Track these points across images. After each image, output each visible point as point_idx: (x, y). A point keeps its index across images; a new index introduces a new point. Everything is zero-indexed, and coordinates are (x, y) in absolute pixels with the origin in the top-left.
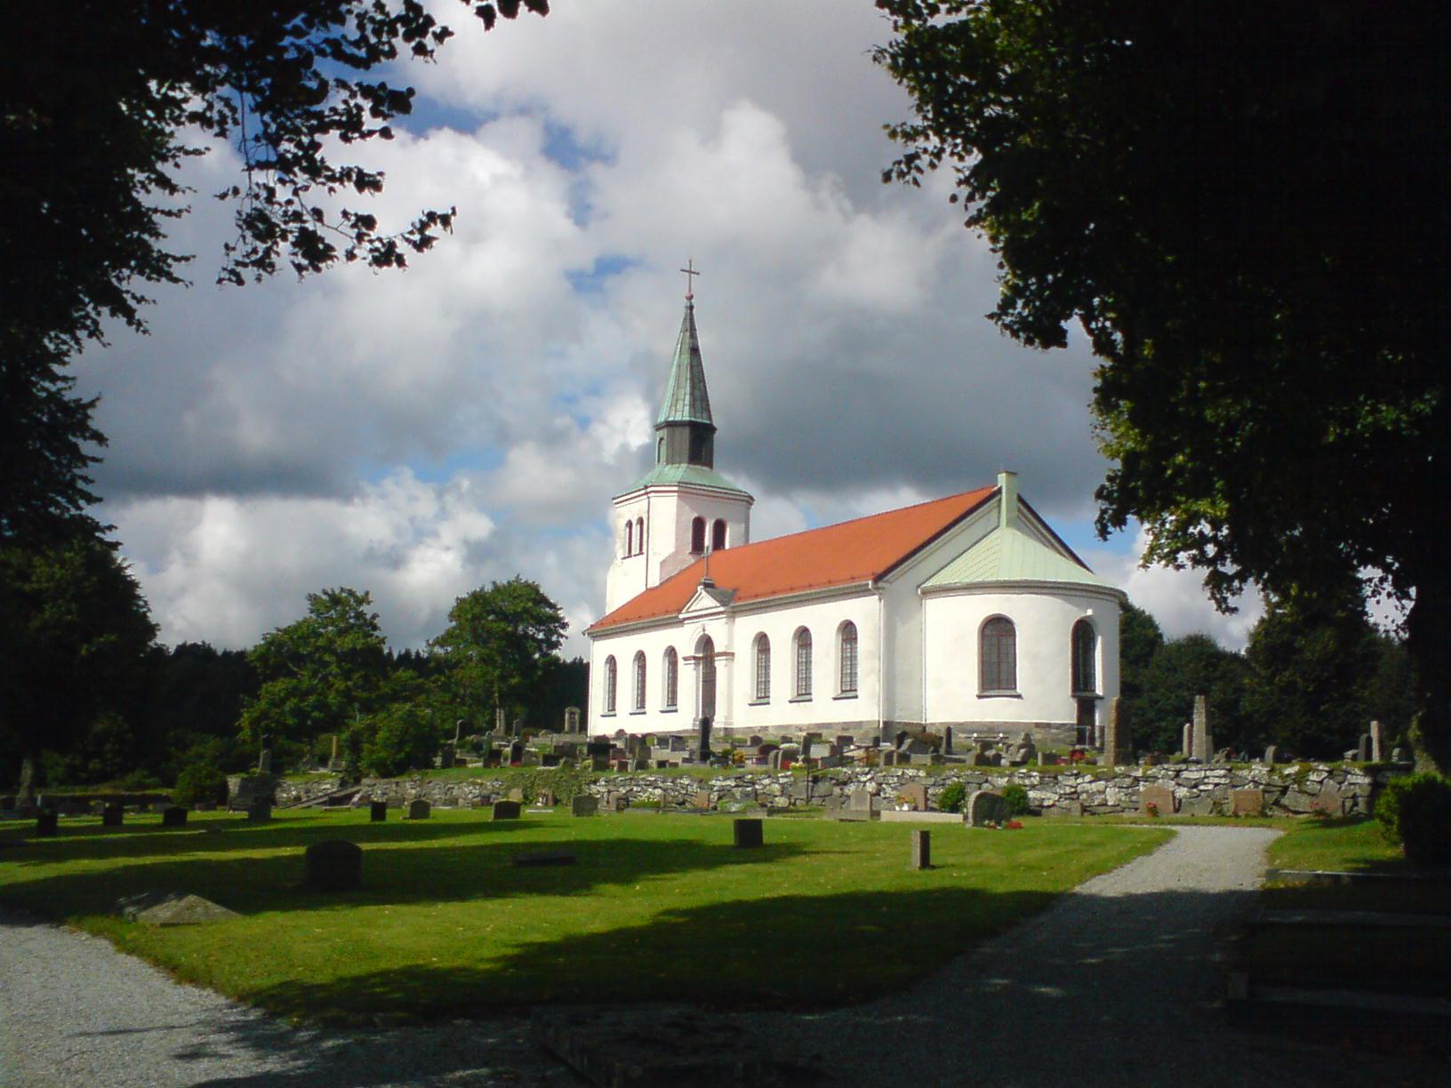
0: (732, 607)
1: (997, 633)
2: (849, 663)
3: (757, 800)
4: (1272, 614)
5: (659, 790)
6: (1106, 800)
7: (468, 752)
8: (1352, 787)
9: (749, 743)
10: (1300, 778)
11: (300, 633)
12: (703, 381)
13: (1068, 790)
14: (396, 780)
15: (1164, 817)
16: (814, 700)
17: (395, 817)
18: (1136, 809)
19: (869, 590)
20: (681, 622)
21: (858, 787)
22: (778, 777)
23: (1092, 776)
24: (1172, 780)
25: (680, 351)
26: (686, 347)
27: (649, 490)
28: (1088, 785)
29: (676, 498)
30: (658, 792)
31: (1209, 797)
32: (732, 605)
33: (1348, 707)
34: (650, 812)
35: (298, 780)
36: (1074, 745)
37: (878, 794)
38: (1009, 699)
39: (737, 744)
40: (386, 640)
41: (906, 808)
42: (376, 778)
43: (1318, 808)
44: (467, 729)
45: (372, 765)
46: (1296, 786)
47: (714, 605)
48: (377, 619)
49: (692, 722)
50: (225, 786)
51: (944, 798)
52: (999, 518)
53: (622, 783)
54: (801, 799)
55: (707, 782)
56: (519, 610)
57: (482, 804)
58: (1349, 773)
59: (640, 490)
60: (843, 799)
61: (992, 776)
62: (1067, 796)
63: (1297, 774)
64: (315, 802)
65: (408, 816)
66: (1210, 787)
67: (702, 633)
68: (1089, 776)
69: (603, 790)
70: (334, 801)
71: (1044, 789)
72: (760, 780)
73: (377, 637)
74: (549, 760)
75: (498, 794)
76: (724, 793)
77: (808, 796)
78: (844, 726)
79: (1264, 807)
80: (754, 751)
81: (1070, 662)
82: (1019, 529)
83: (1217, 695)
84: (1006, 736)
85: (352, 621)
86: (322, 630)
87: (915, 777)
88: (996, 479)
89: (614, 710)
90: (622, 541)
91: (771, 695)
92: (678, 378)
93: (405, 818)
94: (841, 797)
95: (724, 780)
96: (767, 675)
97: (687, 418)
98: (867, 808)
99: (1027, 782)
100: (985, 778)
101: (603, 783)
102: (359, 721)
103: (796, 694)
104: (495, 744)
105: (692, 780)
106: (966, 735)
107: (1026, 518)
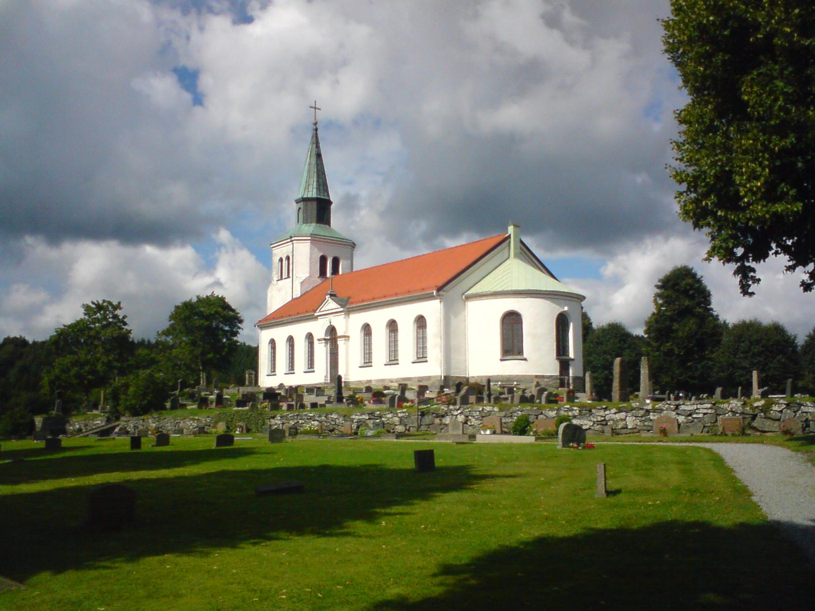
0: (348, 308)
1: (512, 321)
2: (393, 344)
3: (384, 428)
4: (659, 310)
5: (316, 422)
6: (626, 425)
7: (186, 399)
8: (805, 414)
9: (364, 391)
10: (766, 409)
11: (78, 327)
12: (324, 173)
13: (599, 419)
14: (142, 417)
15: (670, 436)
16: (428, 361)
17: (148, 445)
18: (648, 431)
19: (434, 296)
20: (316, 318)
21: (452, 418)
22: (398, 413)
23: (617, 409)
24: (674, 411)
25: (310, 156)
26: (314, 153)
27: (293, 239)
28: (614, 415)
29: (309, 244)
30: (316, 423)
31: (700, 422)
32: (348, 307)
33: (703, 363)
34: (315, 438)
35: (79, 418)
36: (558, 388)
37: (466, 423)
38: (520, 361)
39: (356, 391)
40: (132, 332)
41: (488, 432)
42: (129, 416)
43: (785, 429)
44: (184, 385)
45: (127, 408)
46: (762, 414)
47: (337, 307)
48: (126, 319)
49: (324, 378)
50: (33, 423)
51: (515, 425)
52: (509, 253)
53: (292, 418)
54: (413, 427)
55: (349, 417)
56: (213, 312)
57: (199, 433)
58: (802, 405)
59: (287, 239)
60: (441, 427)
61: (545, 410)
62: (599, 423)
63: (763, 406)
64: (91, 432)
65: (155, 443)
66: (701, 416)
67: (329, 324)
68: (614, 409)
69: (279, 422)
70: (105, 433)
71: (582, 418)
72: (385, 415)
73: (126, 329)
74: (240, 403)
75: (210, 426)
76: (360, 424)
77: (418, 424)
78: (420, 379)
79: (744, 429)
80: (370, 395)
81: (555, 337)
82: (521, 260)
83: (627, 359)
84: (518, 383)
85: (111, 320)
86: (92, 326)
87: (491, 411)
88: (507, 230)
89: (274, 371)
90: (277, 270)
91: (373, 361)
92: (309, 172)
93: (153, 446)
94: (440, 425)
95: (361, 415)
96: (370, 349)
97: (315, 196)
98: (460, 432)
99: (570, 414)
100: (541, 411)
101: (279, 418)
102: (118, 381)
103: (388, 360)
104: (203, 394)
105: (339, 415)
106: (494, 383)
107: (526, 254)
